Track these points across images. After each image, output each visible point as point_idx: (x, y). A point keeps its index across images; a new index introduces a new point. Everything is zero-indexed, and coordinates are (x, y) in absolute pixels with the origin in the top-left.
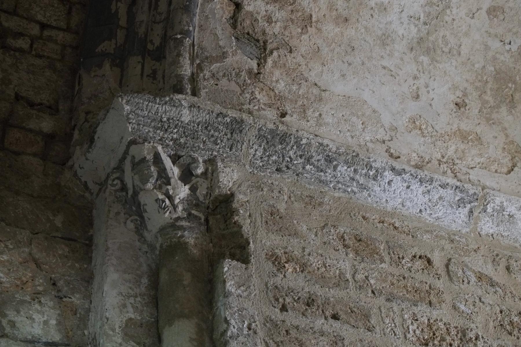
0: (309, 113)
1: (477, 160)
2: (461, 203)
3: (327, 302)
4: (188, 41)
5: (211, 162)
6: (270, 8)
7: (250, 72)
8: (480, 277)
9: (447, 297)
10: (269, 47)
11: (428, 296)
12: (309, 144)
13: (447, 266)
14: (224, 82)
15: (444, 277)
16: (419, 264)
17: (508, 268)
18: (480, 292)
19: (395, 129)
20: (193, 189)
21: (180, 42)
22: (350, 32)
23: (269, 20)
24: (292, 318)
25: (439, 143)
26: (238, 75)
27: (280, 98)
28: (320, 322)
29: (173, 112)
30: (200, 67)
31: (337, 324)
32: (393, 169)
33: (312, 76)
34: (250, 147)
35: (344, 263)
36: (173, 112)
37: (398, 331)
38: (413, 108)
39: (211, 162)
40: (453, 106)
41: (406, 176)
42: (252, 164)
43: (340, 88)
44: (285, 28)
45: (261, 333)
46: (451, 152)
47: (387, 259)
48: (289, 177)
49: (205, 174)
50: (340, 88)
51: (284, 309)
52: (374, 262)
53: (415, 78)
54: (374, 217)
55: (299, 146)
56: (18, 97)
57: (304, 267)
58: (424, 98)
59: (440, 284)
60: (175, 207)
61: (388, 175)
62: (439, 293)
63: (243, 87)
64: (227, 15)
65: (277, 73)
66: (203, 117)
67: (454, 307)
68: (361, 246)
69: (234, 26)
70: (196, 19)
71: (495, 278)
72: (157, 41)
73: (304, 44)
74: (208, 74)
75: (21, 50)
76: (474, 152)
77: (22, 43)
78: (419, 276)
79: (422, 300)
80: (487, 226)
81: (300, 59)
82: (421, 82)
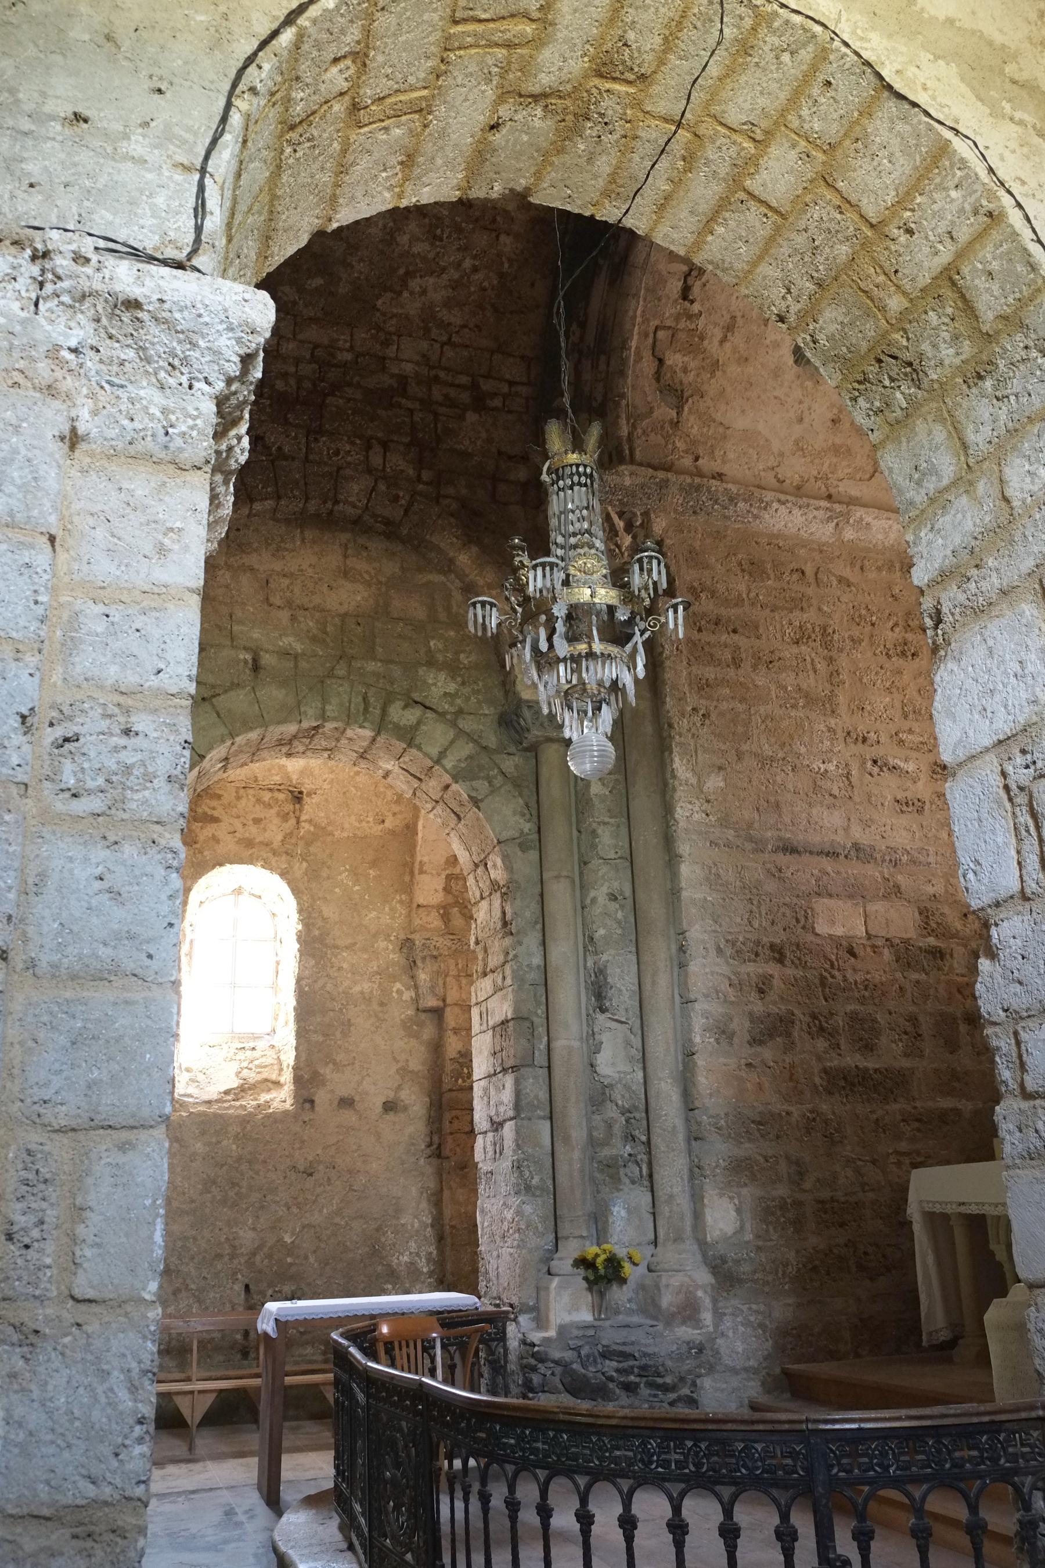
0: (717, 453)
1: (846, 471)
2: (830, 519)
3: (729, 620)
4: (624, 402)
5: (646, 514)
6: (686, 359)
7: (671, 421)
8: (841, 580)
9: (814, 602)
10: (686, 395)
11: (799, 603)
12: (717, 491)
13: (816, 574)
14: (652, 436)
15: (814, 585)
16: (796, 576)
17: (862, 568)
18: (839, 593)
19: (782, 454)
20: (634, 537)
21: (617, 404)
22: (750, 370)
23: (685, 370)
24: (705, 637)
25: (817, 461)
26: (662, 427)
27: (694, 442)
28: (724, 637)
29: (618, 480)
30: (634, 427)
31: (736, 637)
32: (779, 501)
33: (719, 417)
34: (673, 497)
35: (741, 585)
36: (618, 480)
37: (778, 636)
38: (797, 430)
39: (646, 514)
40: (829, 424)
41: (789, 505)
42: (675, 511)
43: (741, 423)
44: (698, 375)
45: (685, 652)
46: (825, 468)
47: (772, 576)
48: (702, 518)
49: (642, 524)
50: (741, 423)
51: (700, 630)
52: (763, 581)
53: (801, 402)
54: (764, 541)
55: (709, 492)
56: (500, 453)
57: (713, 593)
58: (806, 420)
59: (810, 591)
60: (622, 554)
61: (775, 505)
62: (810, 598)
63: (667, 437)
64: (653, 371)
65: (692, 418)
66: (640, 480)
67: (820, 609)
68: (754, 569)
69: (658, 380)
70: (629, 381)
71: (852, 580)
72: (600, 399)
73: (712, 388)
74: (640, 431)
75: (496, 409)
76: (844, 463)
77: (497, 402)
78: (795, 587)
79: (796, 607)
80: (849, 534)
81: (709, 403)
82: (806, 405)
